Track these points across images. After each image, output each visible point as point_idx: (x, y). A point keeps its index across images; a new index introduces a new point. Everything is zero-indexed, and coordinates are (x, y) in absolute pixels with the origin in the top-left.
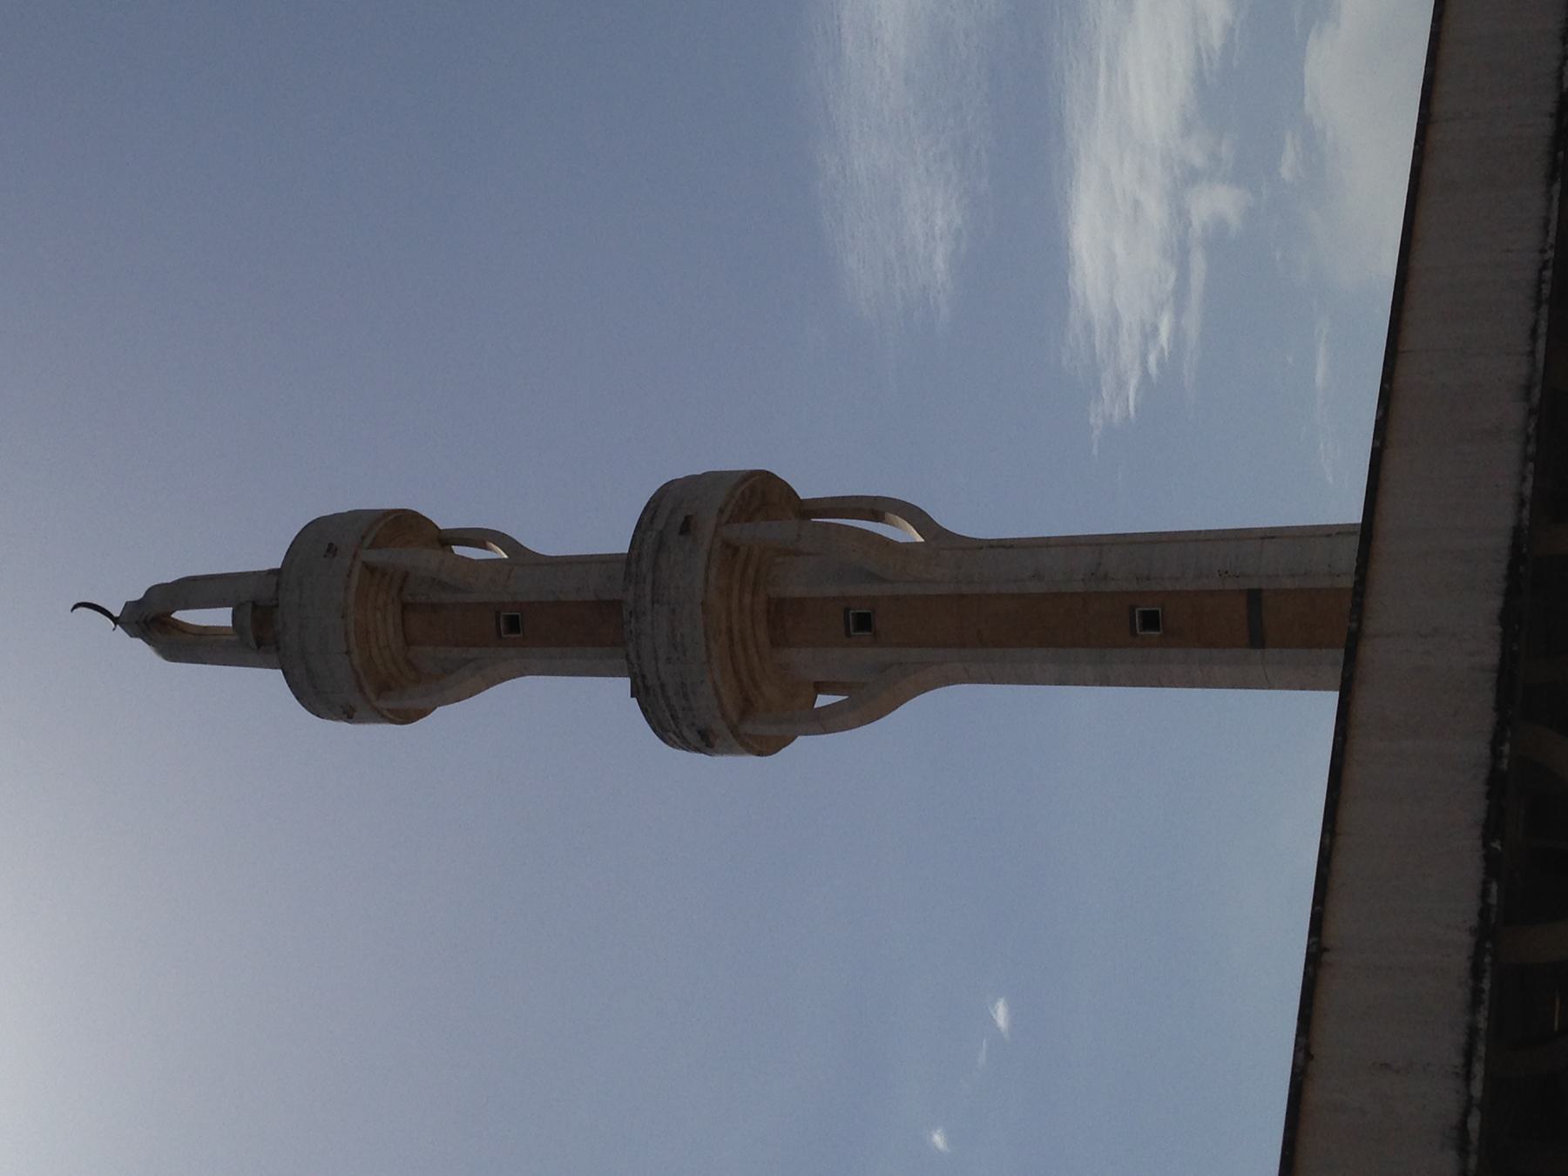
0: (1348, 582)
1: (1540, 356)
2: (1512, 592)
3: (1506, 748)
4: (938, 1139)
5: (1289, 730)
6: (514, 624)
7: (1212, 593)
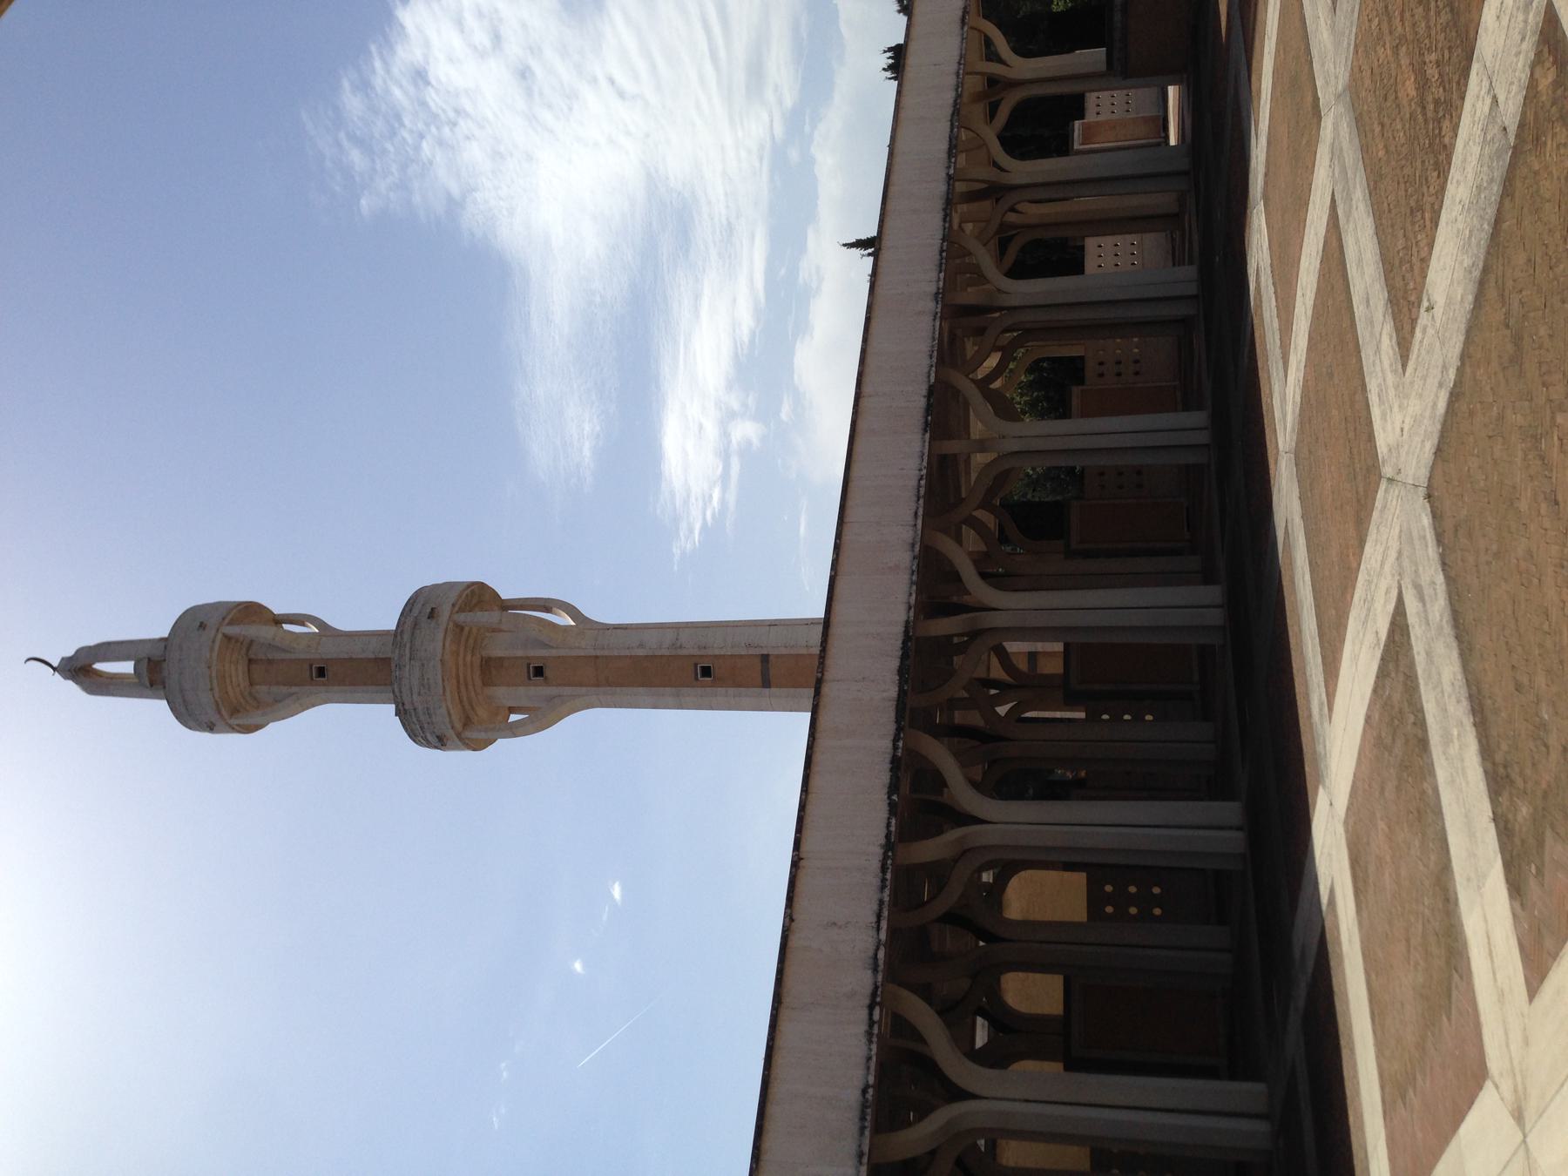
0: (816, 650)
2: (904, 657)
3: (901, 744)
4: (578, 966)
6: (321, 672)
7: (741, 656)
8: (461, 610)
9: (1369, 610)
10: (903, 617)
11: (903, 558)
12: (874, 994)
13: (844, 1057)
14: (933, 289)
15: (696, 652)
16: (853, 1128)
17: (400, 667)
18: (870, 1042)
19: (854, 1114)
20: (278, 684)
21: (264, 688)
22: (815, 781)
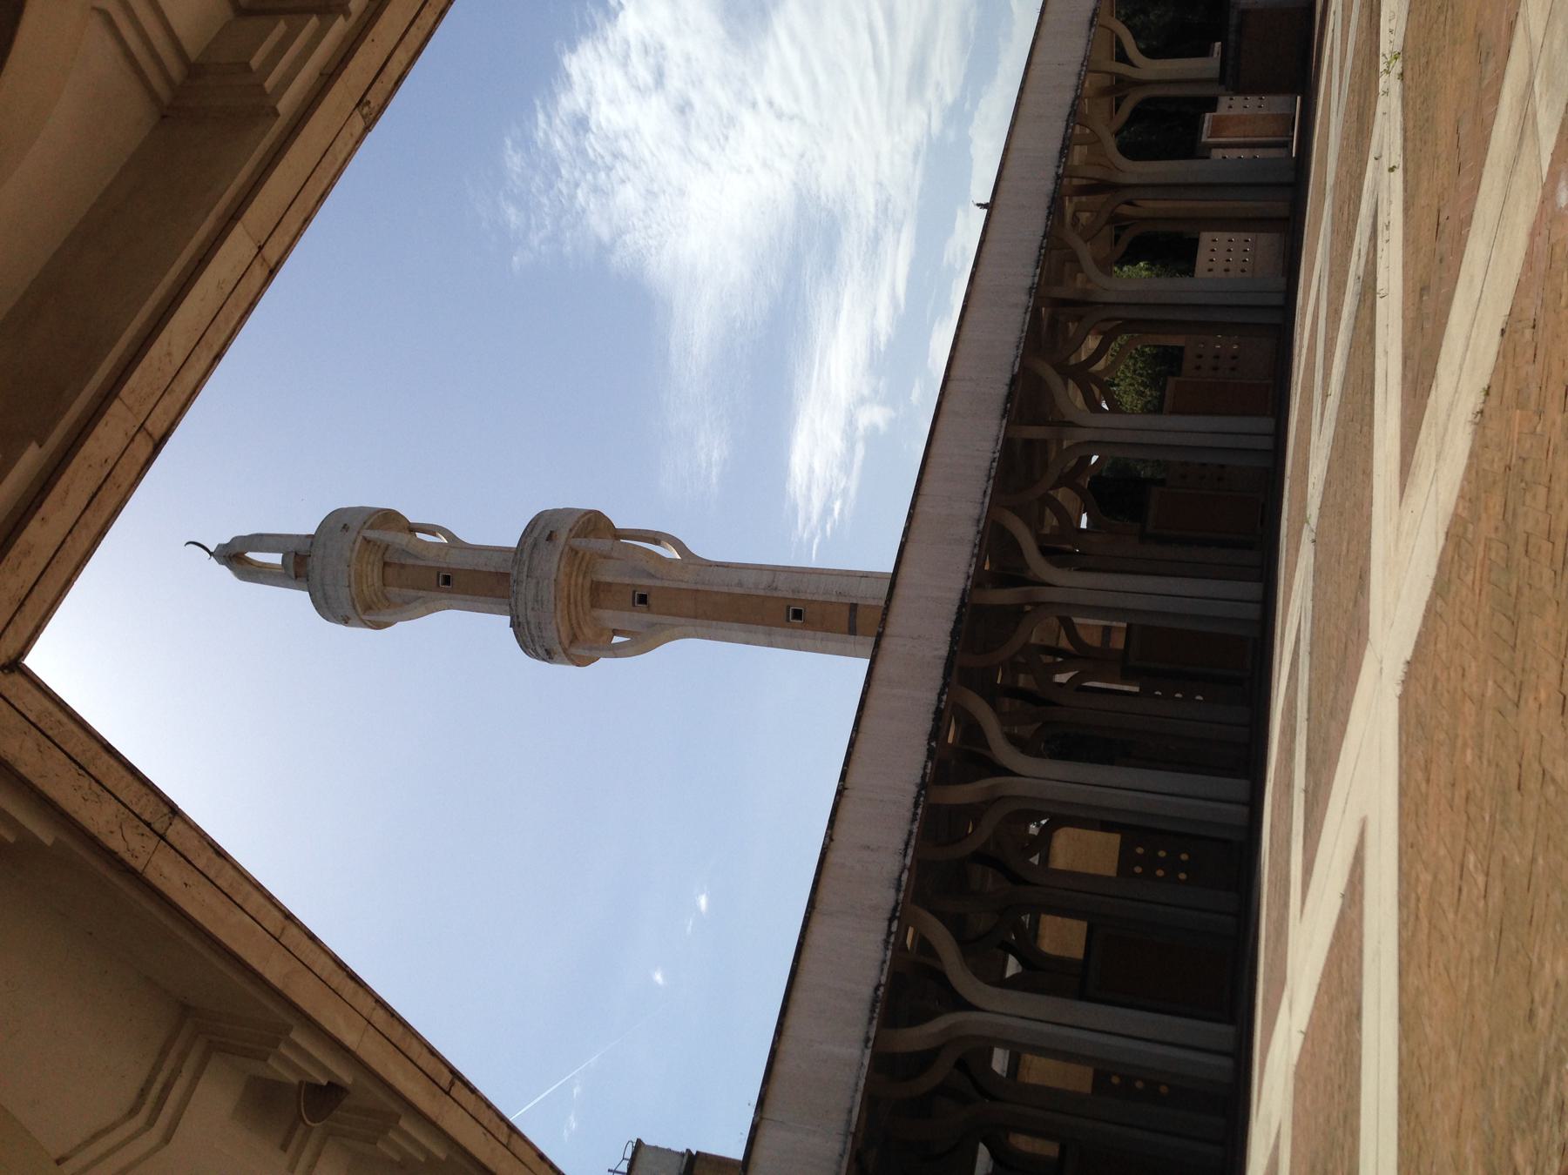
2: (958, 621)
5: (839, 677)
8: (577, 536)
10: (961, 586)
11: (969, 532)
12: (895, 909)
13: (862, 959)
14: (1028, 282)
15: (790, 596)
18: (886, 948)
19: (866, 1006)
20: (408, 587)
21: (396, 590)
22: (865, 722)
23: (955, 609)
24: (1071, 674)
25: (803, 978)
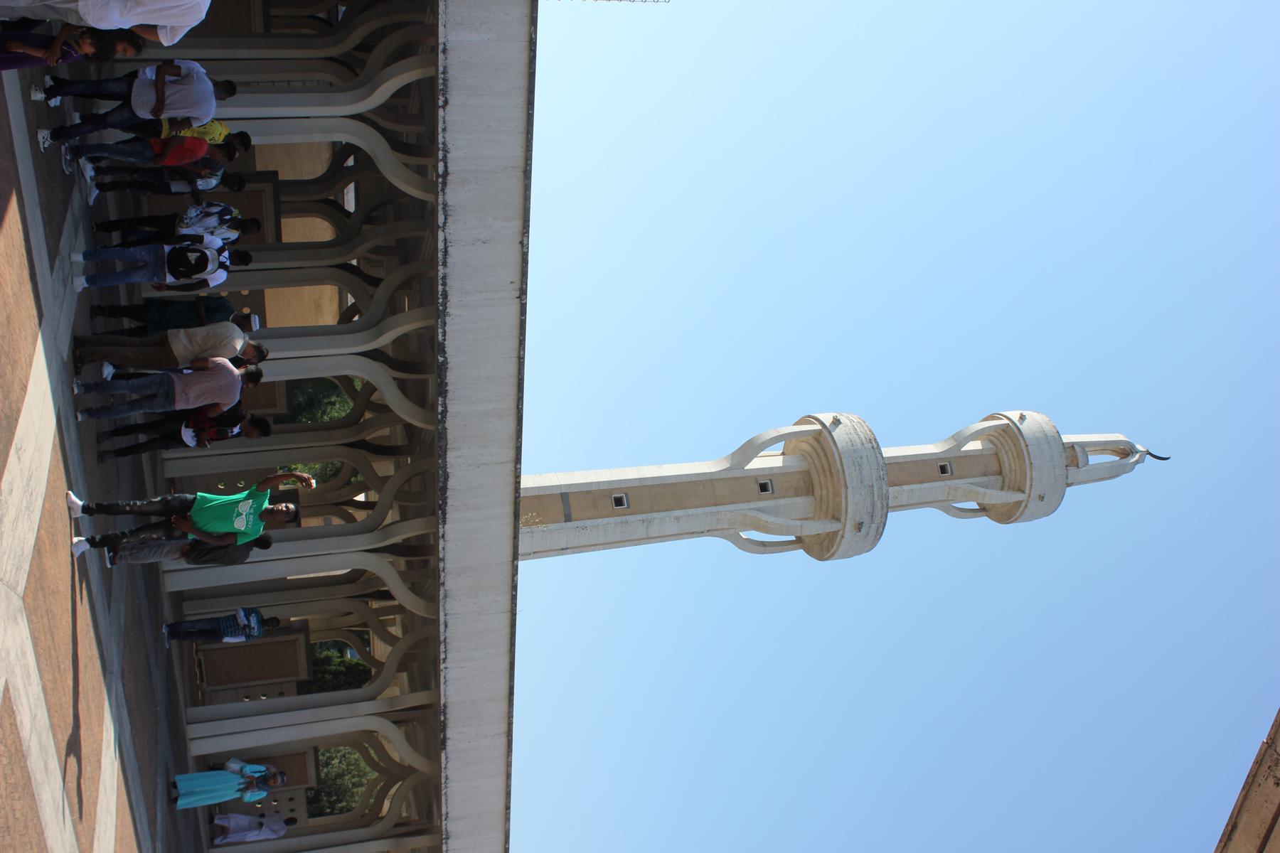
0: (523, 530)
1: (442, 614)
8: (835, 533)
9: (28, 484)
10: (447, 526)
12: (444, 184)
13: (463, 129)
15: (629, 518)
16: (452, 74)
17: (880, 479)
18: (445, 68)
23: (450, 502)
24: (154, 230)
25: (521, 99)
